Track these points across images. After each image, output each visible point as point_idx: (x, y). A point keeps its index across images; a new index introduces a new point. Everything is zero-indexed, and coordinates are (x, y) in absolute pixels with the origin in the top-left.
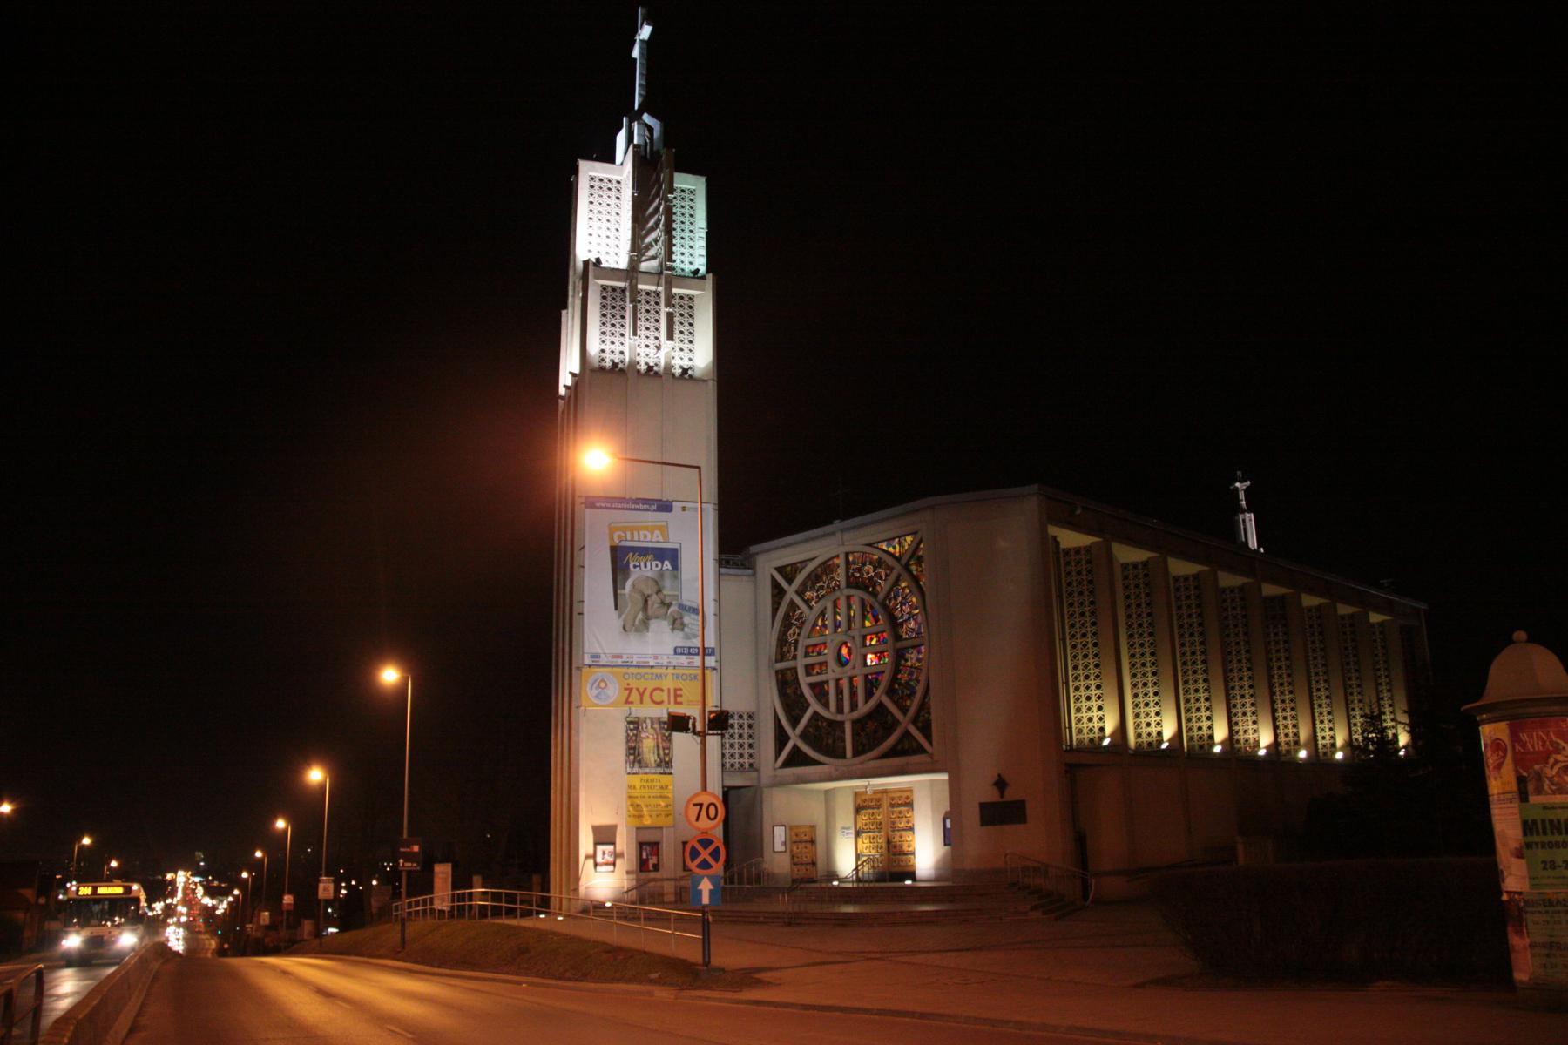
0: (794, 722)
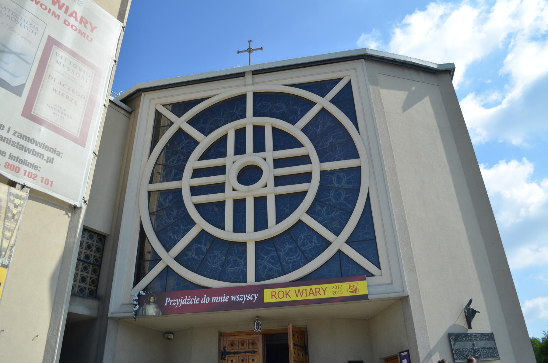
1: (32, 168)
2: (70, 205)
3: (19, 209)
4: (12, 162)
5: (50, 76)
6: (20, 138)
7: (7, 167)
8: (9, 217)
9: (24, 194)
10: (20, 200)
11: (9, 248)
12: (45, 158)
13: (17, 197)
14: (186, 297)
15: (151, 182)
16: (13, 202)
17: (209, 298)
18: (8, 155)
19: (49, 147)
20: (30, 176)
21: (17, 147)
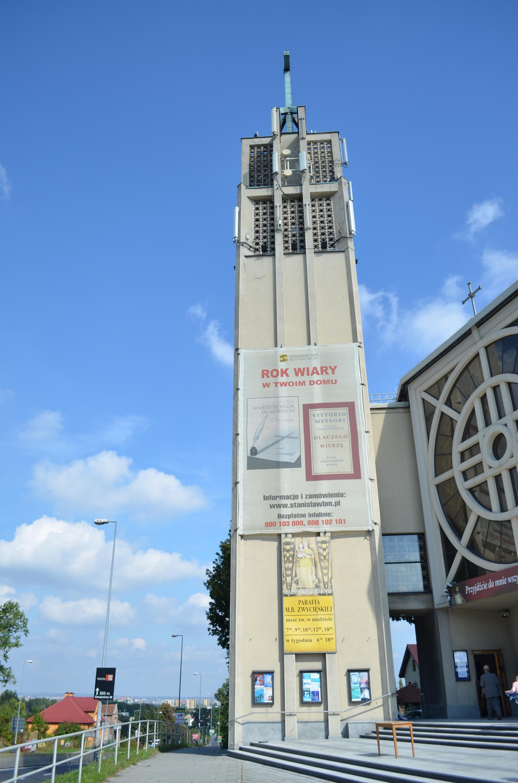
0: (459, 534)
1: (327, 516)
2: (366, 531)
3: (327, 551)
4: (312, 519)
5: (315, 437)
6: (311, 498)
7: (309, 524)
8: (322, 559)
9: (327, 538)
10: (325, 544)
11: (329, 581)
12: (333, 504)
13: (323, 542)
14: (478, 583)
15: (436, 475)
16: (321, 548)
17: (493, 582)
18: (307, 515)
19: (333, 494)
20: (327, 523)
21: (311, 506)
